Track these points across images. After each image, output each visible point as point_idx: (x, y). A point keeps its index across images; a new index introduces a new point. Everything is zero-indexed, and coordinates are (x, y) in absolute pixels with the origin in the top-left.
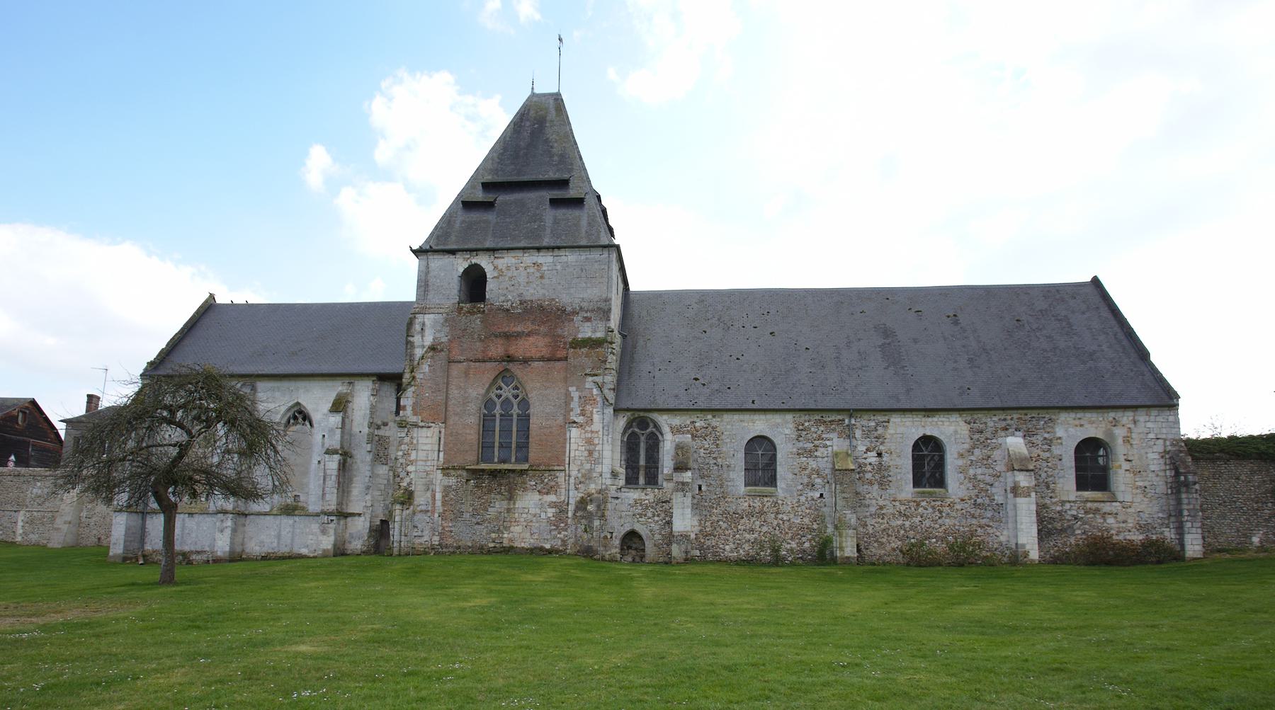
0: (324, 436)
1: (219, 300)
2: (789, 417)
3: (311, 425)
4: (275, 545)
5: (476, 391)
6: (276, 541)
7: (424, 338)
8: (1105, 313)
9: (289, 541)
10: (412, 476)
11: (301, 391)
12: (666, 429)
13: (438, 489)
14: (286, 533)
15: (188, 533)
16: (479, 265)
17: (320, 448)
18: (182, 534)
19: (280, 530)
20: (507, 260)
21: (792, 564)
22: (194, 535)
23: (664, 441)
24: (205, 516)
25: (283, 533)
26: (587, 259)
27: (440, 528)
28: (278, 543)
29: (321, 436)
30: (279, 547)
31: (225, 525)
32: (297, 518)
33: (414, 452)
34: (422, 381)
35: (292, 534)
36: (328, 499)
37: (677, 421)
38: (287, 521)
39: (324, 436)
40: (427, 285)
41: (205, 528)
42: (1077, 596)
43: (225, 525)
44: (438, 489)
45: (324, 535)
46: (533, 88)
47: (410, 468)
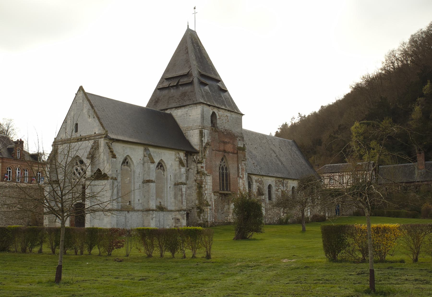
1: (243, 117)
2: (274, 179)
3: (164, 170)
9: (163, 223)
10: (207, 195)
12: (254, 181)
13: (213, 200)
14: (122, 219)
15: (128, 221)
18: (126, 221)
21: (291, 224)
22: (130, 222)
23: (252, 185)
24: (134, 212)
25: (161, 219)
27: (214, 216)
28: (159, 224)
31: (153, 216)
32: (165, 213)
34: (207, 157)
38: (161, 214)
41: (134, 218)
42: (309, 229)
43: (153, 216)
45: (184, 219)
46: (188, 26)
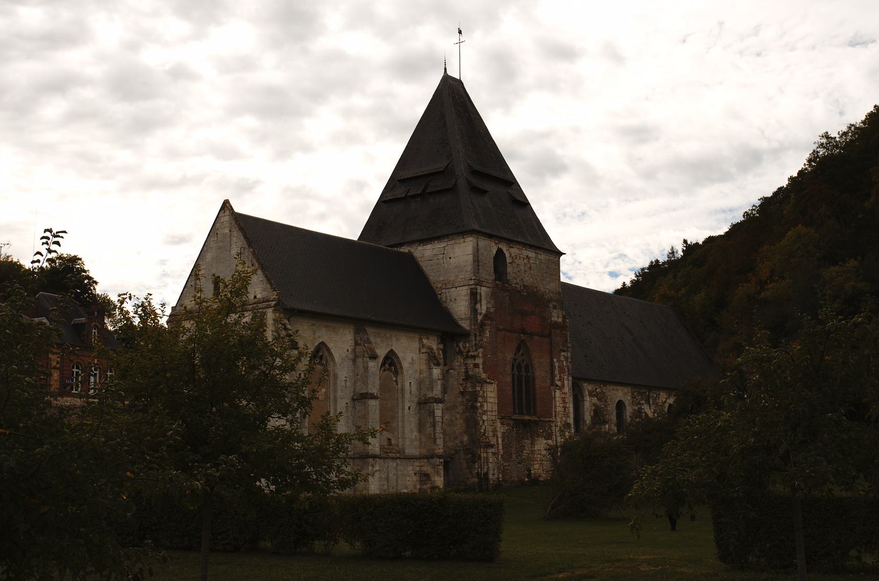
0: (410, 383)
4: (386, 487)
5: (509, 356)
6: (386, 484)
7: (482, 307)
8: (212, 231)
11: (394, 339)
16: (502, 250)
17: (409, 395)
19: (388, 473)
20: (515, 251)
25: (390, 475)
26: (549, 259)
29: (409, 383)
30: (388, 489)
31: (375, 469)
33: (486, 403)
35: (396, 477)
36: (438, 444)
37: (590, 387)
39: (410, 383)
40: (478, 261)
43: (375, 469)
44: (500, 435)
47: (485, 417)
